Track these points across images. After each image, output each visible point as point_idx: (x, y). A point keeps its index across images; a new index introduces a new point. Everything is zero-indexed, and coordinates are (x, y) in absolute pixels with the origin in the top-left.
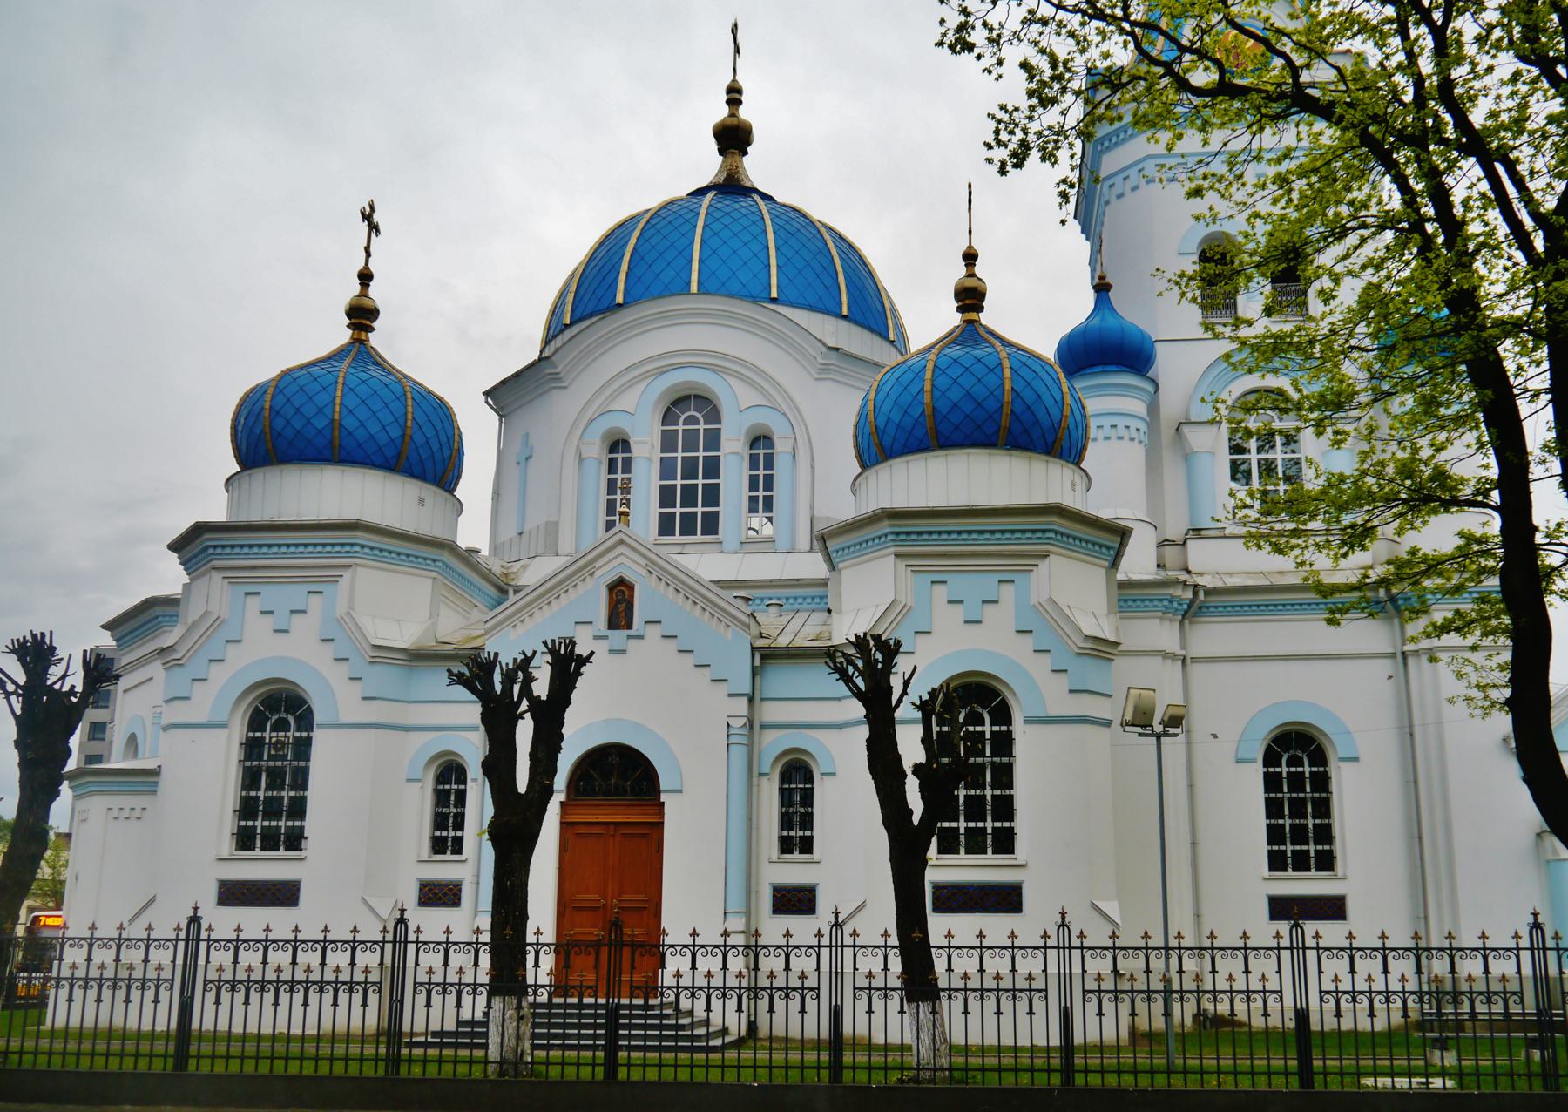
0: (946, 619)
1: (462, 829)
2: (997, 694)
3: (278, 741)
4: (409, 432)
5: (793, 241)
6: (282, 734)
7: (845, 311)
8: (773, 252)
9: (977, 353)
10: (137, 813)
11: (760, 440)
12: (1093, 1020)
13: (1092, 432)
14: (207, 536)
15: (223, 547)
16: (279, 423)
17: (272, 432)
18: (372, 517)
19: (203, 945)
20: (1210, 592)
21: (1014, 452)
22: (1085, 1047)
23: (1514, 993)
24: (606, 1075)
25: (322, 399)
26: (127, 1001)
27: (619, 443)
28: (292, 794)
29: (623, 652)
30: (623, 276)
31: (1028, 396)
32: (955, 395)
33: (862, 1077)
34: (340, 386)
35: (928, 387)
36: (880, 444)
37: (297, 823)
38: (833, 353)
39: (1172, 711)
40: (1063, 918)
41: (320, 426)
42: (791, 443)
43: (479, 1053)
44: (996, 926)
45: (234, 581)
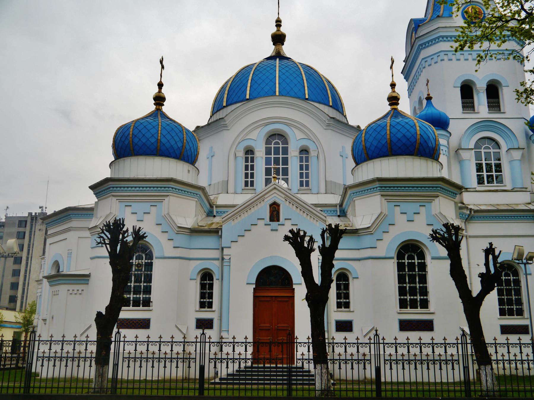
0: (400, 220)
1: (212, 298)
2: (419, 248)
3: (139, 264)
4: (184, 145)
5: (311, 78)
6: (140, 261)
7: (331, 104)
8: (305, 81)
9: (398, 120)
10: (80, 292)
11: (304, 151)
12: (388, 371)
13: (441, 152)
14: (110, 183)
15: (117, 187)
16: (136, 140)
17: (129, 143)
18: (179, 177)
19: (37, 343)
20: (476, 211)
21: (421, 158)
22: (385, 383)
23: (456, 360)
24: (377, 395)
25: (153, 131)
26: (78, 366)
27: (249, 152)
28: (145, 284)
29: (277, 230)
30: (248, 88)
31: (425, 136)
32: (399, 136)
33: (389, 394)
34: (160, 126)
35: (388, 133)
36: (364, 153)
37: (147, 296)
38: (332, 119)
39: (530, 255)
40: (376, 332)
41: (153, 142)
42: (317, 153)
43: (312, 387)
44: (142, 334)
45: (121, 201)
